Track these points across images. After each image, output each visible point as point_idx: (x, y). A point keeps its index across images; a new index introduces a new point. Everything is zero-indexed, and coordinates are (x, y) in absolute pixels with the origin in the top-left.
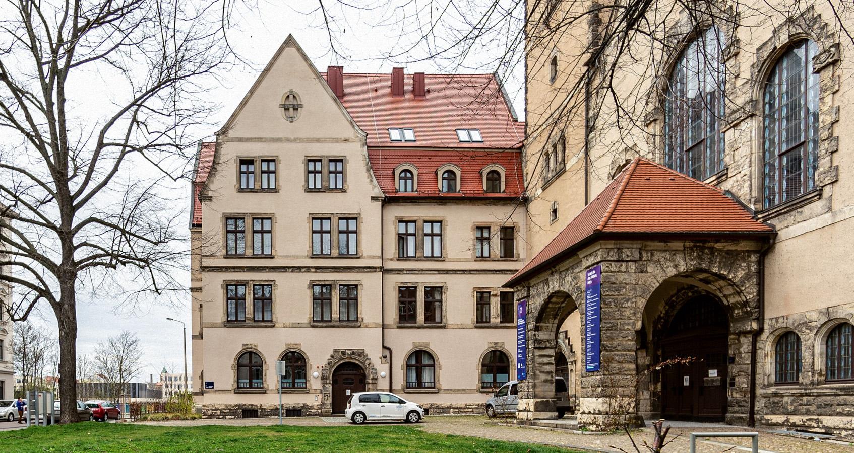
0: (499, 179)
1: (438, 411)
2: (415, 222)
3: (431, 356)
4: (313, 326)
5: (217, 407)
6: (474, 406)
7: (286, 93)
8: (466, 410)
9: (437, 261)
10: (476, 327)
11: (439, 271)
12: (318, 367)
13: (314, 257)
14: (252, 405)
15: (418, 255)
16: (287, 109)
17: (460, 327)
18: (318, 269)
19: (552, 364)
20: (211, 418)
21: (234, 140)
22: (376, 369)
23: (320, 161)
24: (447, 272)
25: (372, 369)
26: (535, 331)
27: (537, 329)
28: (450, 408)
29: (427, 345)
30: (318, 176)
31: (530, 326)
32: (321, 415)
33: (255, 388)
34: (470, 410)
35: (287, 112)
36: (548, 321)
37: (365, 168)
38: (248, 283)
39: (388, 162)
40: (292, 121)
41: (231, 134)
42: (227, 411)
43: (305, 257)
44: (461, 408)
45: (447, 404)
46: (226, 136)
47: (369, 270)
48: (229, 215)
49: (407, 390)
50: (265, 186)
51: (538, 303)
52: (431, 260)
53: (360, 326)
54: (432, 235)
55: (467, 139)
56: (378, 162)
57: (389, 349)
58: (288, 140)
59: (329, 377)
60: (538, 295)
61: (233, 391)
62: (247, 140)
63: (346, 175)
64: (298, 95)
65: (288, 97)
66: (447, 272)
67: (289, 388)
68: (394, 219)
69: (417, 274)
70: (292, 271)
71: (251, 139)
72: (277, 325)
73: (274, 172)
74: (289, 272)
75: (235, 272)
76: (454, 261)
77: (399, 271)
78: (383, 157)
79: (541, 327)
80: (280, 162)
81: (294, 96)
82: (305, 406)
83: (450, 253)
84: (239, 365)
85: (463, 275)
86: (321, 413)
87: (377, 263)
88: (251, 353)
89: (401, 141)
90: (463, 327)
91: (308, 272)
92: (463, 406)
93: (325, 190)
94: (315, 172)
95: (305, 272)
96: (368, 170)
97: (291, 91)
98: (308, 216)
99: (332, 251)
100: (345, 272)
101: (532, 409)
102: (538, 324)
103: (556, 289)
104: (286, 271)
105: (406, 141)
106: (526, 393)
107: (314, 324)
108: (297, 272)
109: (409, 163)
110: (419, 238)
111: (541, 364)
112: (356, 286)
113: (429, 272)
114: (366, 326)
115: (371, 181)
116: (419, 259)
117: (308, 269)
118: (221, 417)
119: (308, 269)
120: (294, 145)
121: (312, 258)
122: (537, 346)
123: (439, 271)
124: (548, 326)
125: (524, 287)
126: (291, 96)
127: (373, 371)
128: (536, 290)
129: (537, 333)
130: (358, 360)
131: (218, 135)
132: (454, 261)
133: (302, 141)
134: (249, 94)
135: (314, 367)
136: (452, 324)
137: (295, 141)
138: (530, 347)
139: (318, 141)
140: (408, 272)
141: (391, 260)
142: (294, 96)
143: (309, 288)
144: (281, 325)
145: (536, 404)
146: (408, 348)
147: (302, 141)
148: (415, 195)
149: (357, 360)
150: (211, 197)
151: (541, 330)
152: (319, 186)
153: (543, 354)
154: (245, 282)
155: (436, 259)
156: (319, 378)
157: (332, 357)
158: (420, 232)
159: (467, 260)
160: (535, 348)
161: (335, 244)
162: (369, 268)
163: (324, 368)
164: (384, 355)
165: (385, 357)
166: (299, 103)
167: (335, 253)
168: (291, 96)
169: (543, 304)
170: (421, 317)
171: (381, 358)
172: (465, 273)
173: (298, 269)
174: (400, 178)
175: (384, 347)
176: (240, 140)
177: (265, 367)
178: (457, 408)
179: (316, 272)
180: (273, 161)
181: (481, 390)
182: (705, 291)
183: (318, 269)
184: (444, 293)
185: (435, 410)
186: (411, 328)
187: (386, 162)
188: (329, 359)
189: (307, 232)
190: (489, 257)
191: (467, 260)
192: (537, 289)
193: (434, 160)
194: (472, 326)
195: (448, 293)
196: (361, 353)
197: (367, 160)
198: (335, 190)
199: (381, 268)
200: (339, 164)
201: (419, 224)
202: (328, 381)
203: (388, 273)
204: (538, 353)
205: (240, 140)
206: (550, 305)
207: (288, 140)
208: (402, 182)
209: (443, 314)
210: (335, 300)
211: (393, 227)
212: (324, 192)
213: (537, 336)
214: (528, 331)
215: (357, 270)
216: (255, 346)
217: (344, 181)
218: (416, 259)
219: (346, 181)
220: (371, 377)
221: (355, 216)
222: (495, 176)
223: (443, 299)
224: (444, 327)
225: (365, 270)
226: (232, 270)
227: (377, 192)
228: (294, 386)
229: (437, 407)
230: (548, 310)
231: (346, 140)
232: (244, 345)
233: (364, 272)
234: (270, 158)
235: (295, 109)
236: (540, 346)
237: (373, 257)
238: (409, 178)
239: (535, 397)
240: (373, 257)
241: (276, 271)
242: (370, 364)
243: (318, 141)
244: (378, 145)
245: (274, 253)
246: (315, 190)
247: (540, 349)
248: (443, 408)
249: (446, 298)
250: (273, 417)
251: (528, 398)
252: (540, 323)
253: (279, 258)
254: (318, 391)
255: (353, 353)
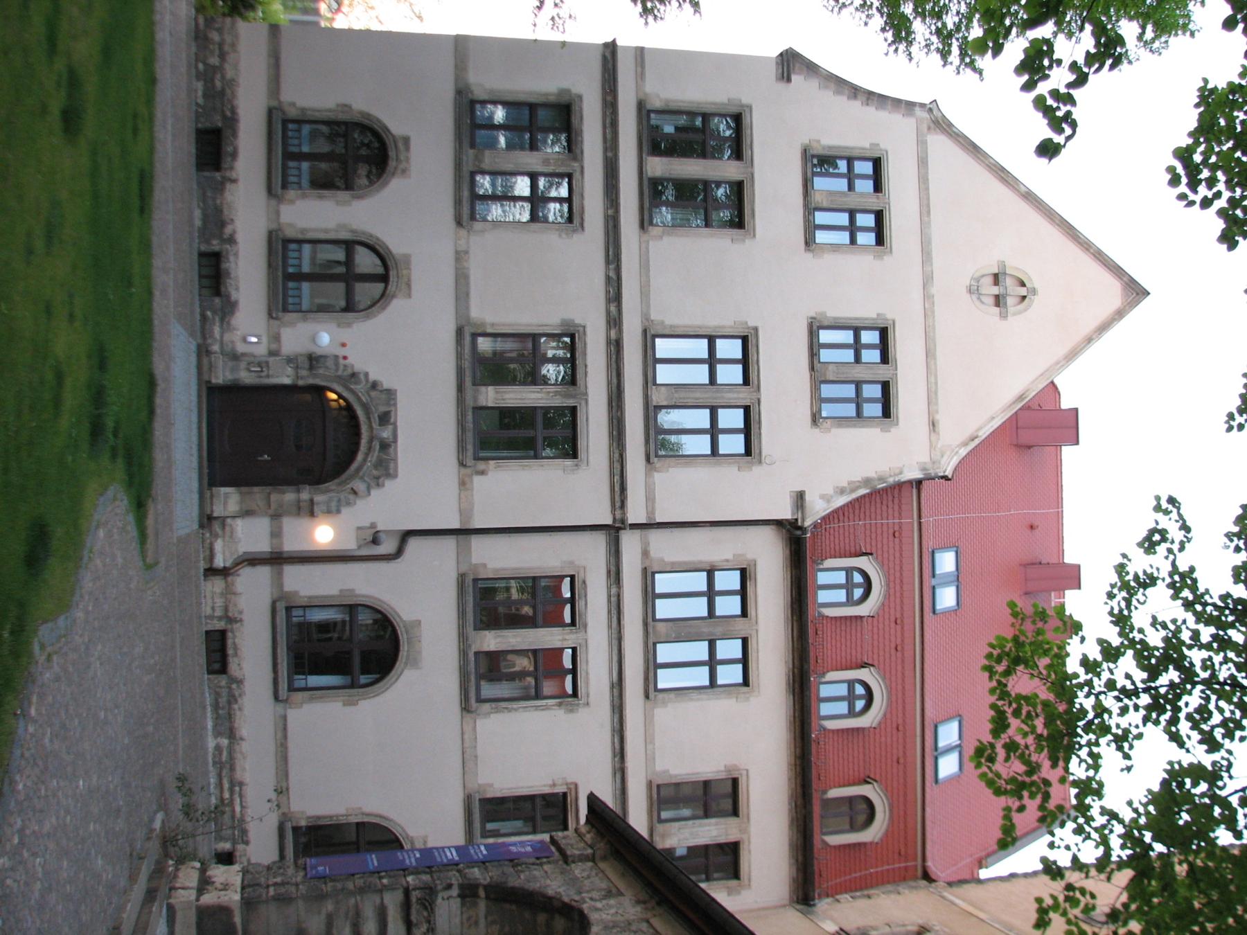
0: (853, 828)
1: (223, 701)
2: (744, 613)
3: (382, 300)
4: (460, 332)
5: (231, 58)
6: (238, 809)
7: (1030, 280)
8: (226, 785)
9: (646, 679)
10: (468, 800)
11: (618, 685)
12: (344, 345)
13: (649, 338)
14: (234, 155)
15: (661, 627)
16: (996, 279)
17: (468, 751)
18: (615, 348)
19: (337, 370)
20: (196, 38)
21: (922, 143)
22: (338, 511)
23: (885, 359)
24: (618, 708)
25: (339, 501)
26: (461, 887)
27: (469, 892)
28: (232, 734)
29: (414, 663)
30: (849, 355)
31: (476, 873)
32: (203, 351)
33: (285, 168)
34: (227, 795)
35: (990, 280)
36: (493, 922)
37: (872, 474)
38: (575, 159)
39: (885, 541)
40: (970, 291)
41: (938, 144)
42: (218, 84)
43: (646, 317)
44: (232, 769)
45: (244, 730)
46: (929, 128)
47: (617, 488)
48: (746, 121)
49: (281, 606)
50: (821, 218)
51: (548, 882)
52: (647, 661)
53: (462, 464)
54: (712, 663)
55: (941, 744)
56: (885, 515)
57: (399, 553)
58: (927, 280)
59: (315, 376)
60: (574, 881)
61: (275, 103)
62: (923, 180)
63: (855, 426)
64: (1025, 310)
65: (1023, 284)
66: (618, 708)
67: (285, 265)
68: (750, 556)
69: (610, 627)
70: (608, 278)
71: (927, 189)
72: (463, 232)
73: (853, 241)
74: (607, 268)
75: (604, 127)
76: (648, 721)
77: (615, 575)
78: (897, 528)
79: (475, 905)
80: (879, 257)
81: (1024, 298)
82: (229, 308)
83: (667, 715)
84: (346, 106)
85: (609, 754)
86: (208, 353)
87: (636, 514)
88: (384, 278)
89: (934, 576)
90: (468, 759)
91: (608, 322)
92: (239, 775)
93: (818, 374)
94: (857, 347)
95: (608, 312)
96: (867, 482)
97: (1034, 291)
98: (751, 324)
99: (663, 388)
100: (611, 420)
101: (208, 899)
102: (482, 893)
103: (593, 916)
104: (608, 262)
105: (934, 588)
106: (263, 880)
107: (466, 333)
108: (608, 292)
109: (887, 596)
110: (705, 628)
111: (358, 914)
112: (574, 454)
113: (615, 658)
114: (462, 484)
115: (842, 491)
116: (650, 630)
117: (614, 321)
118: (201, 66)
119: (614, 321)
120: (917, 294)
121: (645, 332)
122: (415, 895)
123: (618, 685)
124: (476, 923)
125: (591, 847)
126: (1023, 291)
127: (334, 504)
128: (585, 874)
129: (455, 892)
130: (365, 460)
131: (931, 110)
132: (648, 721)
133: (928, 314)
134: (1023, 189)
135: (346, 334)
136: (474, 729)
137: (927, 297)
138: (410, 879)
139: (930, 353)
140: (614, 599)
141: (645, 554)
142: (1024, 298)
143: (565, 323)
144: (462, 244)
145: (224, 910)
146: (403, 609)
147: (928, 314)
148: (811, 613)
149: (367, 455)
150: (789, 80)
151: (463, 904)
152: (825, 355)
153: (390, 919)
154: (578, 151)
155: (651, 675)
156: (311, 348)
157: (374, 385)
158: (718, 630)
159: (650, 759)
160: (407, 892)
161: (682, 395)
162: (623, 489)
163: (342, 361)
164: (382, 536)
165: (375, 541)
166: (1011, 310)
167: (657, 397)
168: (1023, 291)
169: (544, 896)
170: (492, 641)
171: (373, 526)
172: (614, 756)
173: (615, 296)
174: (849, 571)
175: (407, 535)
176: (923, 162)
177: (343, 195)
178: (231, 758)
179: (609, 342)
180: (880, 241)
181: (289, 826)
182: (982, 302)
183: (615, 348)
184: (560, 705)
185: (224, 692)
186: (462, 614)
187: (885, 535)
188: (366, 375)
189: (712, 321)
190: (660, 821)
191: (650, 759)
192: (588, 877)
193: (893, 658)
194: (472, 786)
195: (560, 714)
196: (385, 469)
197: (891, 480)
198: (818, 400)
199: (623, 521)
200: (877, 409)
201: (741, 626)
202: (304, 373)
203: (608, 544)
204: (393, 901)
205: (923, 162)
206: (542, 918)
207: (927, 280)
208: (841, 578)
209: (503, 704)
210: (533, 396)
211: (730, 556)
212: (812, 368)
213: (446, 894)
214: (459, 871)
215: (617, 455)
216: (404, 171)
217: (841, 421)
218: (650, 619)
219: (840, 426)
220: (318, 498)
221: (755, 450)
222: (862, 818)
223: (544, 702)
224: (466, 708)
225: (617, 478)
226: (608, 121)
227: (818, 508)
228: (289, 277)
229: (232, 699)
230: (527, 915)
231: (933, 425)
232: (406, 140)
233: (612, 475)
234: (886, 232)
235: (998, 301)
236: (415, 908)
237: (650, 499)
238: (849, 595)
239: (248, 904)
240: (650, 499)
241: (607, 234)
242: (355, 493)
243: (930, 353)
244: (923, 515)
245: (654, 231)
246: (814, 347)
247: (406, 906)
248: (230, 717)
249: (547, 708)
250: (197, 213)
251: (243, 888)
252: (487, 898)
253: (643, 246)
254: (274, 346)
255: (385, 446)
